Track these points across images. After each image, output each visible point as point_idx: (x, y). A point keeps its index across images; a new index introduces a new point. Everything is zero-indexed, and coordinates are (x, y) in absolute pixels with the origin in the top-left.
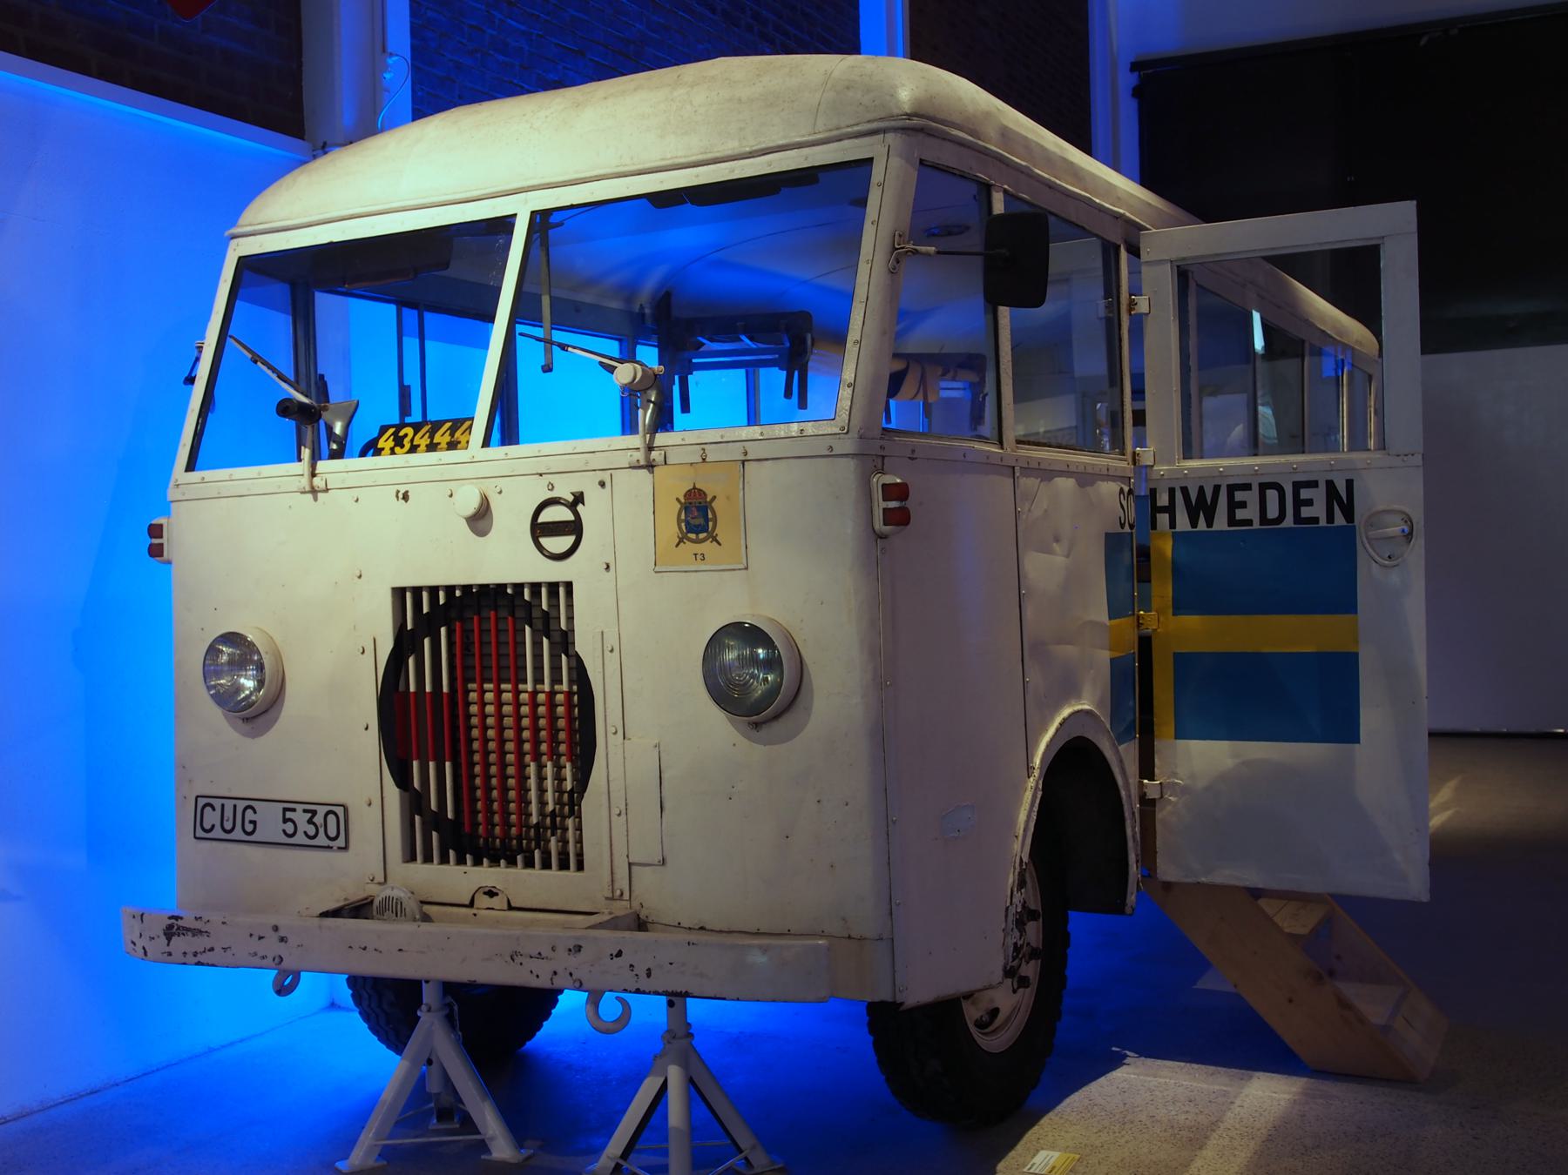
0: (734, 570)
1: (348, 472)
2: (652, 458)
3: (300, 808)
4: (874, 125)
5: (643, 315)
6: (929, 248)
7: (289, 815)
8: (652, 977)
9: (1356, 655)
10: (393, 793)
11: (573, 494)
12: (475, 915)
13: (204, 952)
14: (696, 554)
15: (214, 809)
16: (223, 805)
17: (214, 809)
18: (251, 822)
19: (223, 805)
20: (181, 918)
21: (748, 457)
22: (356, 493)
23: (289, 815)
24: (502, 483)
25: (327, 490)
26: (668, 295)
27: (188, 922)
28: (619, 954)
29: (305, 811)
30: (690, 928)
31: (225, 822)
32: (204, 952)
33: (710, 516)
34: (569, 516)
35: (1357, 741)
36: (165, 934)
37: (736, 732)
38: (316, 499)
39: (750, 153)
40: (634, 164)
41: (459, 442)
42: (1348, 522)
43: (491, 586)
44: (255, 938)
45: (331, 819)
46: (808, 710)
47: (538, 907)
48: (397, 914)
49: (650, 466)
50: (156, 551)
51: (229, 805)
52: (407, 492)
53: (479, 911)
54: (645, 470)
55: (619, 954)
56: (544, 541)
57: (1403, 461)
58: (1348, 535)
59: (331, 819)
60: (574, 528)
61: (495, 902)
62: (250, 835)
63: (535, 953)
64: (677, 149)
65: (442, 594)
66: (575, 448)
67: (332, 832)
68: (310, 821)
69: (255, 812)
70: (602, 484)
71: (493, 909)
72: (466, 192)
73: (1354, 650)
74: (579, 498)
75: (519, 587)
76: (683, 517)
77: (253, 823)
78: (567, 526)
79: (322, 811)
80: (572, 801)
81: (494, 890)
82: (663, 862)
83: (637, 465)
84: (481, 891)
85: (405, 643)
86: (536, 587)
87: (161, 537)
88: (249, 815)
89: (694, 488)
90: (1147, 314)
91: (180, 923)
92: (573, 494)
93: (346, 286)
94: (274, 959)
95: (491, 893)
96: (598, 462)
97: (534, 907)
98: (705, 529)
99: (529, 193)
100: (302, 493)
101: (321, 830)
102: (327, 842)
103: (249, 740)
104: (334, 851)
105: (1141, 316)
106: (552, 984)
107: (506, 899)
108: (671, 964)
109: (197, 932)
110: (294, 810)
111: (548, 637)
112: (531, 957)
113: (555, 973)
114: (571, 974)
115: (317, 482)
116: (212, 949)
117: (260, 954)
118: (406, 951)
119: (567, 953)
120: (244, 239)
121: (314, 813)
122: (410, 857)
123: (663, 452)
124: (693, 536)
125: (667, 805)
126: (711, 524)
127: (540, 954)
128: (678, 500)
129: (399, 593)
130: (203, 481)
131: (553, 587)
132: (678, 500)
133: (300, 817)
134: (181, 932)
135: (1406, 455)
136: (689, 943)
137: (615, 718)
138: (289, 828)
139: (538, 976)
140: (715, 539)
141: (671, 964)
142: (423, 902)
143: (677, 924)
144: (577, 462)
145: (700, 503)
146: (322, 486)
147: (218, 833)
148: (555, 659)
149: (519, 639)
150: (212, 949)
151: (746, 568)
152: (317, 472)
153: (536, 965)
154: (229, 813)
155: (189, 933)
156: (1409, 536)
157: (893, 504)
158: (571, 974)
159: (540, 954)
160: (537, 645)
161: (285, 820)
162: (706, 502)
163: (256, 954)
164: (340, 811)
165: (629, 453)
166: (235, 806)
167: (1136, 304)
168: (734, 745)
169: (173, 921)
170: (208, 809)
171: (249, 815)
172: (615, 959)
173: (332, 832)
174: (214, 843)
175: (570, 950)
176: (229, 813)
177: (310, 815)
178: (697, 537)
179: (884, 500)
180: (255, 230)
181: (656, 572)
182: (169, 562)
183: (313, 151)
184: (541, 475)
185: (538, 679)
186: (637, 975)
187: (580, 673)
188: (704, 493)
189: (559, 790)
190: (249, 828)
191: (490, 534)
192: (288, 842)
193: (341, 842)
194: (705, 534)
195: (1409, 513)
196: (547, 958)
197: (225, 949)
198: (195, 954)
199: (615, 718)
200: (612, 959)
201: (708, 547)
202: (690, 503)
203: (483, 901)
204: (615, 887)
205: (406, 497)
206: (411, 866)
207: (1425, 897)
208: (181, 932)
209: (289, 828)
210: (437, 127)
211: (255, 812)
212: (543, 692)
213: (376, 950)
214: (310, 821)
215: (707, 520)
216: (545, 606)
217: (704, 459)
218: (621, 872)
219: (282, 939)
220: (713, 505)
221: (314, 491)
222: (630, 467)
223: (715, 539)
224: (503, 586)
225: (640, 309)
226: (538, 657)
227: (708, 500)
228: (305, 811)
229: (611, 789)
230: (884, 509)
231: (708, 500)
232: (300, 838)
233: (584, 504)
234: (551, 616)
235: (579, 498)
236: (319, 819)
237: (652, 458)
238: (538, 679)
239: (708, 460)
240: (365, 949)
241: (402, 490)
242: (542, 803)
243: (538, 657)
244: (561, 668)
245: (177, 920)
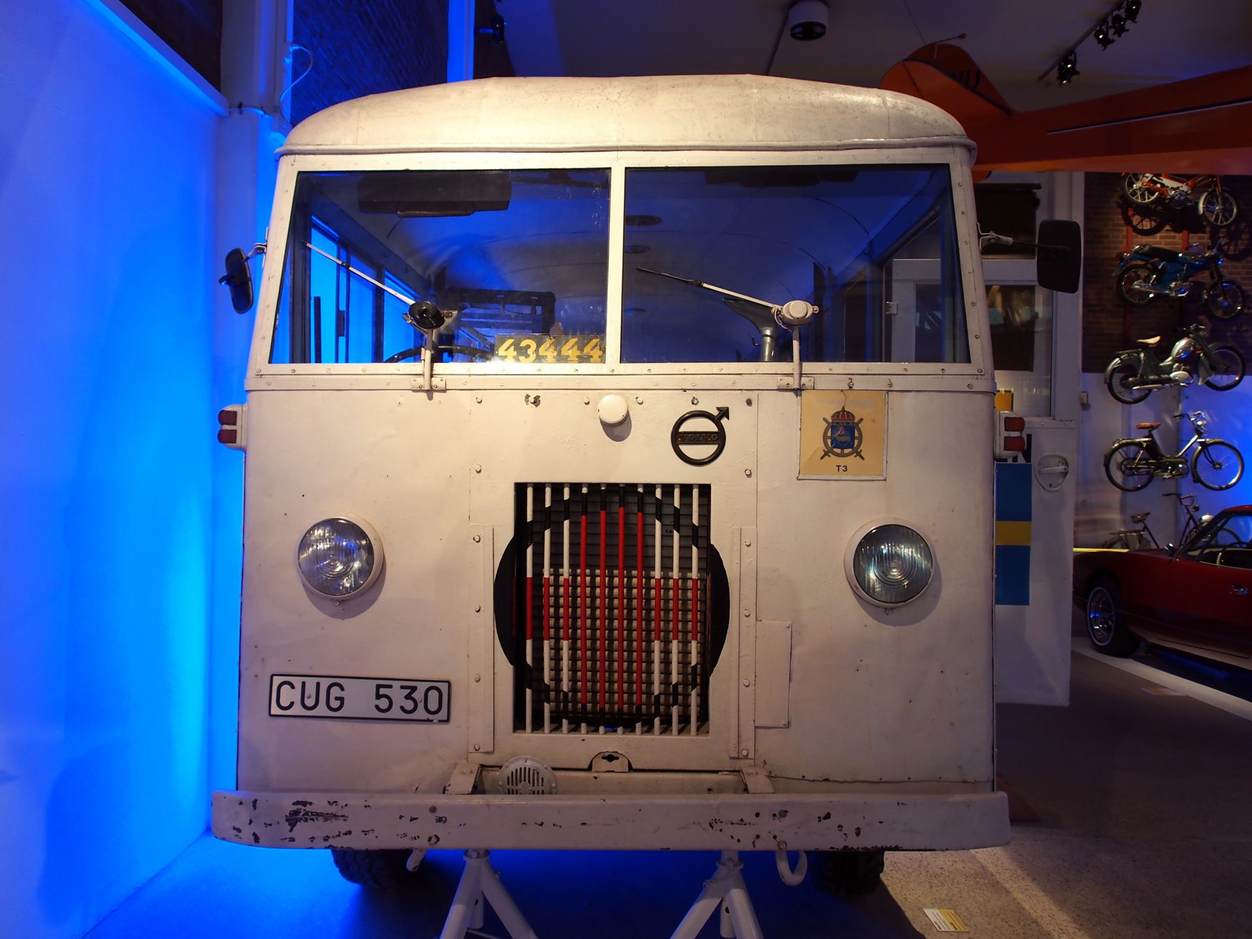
0: (879, 480)
1: (470, 375)
2: (802, 383)
3: (396, 685)
4: (945, 139)
5: (430, 281)
6: (1009, 238)
7: (382, 691)
8: (860, 836)
9: (1029, 547)
10: (506, 670)
11: (718, 409)
12: (596, 778)
13: (339, 836)
14: (839, 466)
15: (293, 687)
16: (304, 684)
17: (293, 687)
18: (337, 698)
19: (304, 684)
20: (311, 804)
21: (892, 389)
22: (480, 394)
23: (382, 691)
24: (642, 396)
25: (444, 391)
26: (445, 268)
27: (319, 803)
28: (828, 816)
29: (402, 687)
30: (814, 780)
31: (306, 699)
32: (339, 836)
33: (856, 435)
34: (712, 427)
35: (1027, 603)
36: (287, 820)
37: (868, 616)
38: (430, 398)
39: (838, 146)
40: (757, 141)
41: (591, 357)
42: (1026, 461)
43: (621, 486)
44: (406, 820)
45: (433, 695)
46: (936, 597)
47: (665, 768)
48: (529, 782)
49: (798, 391)
50: (227, 438)
51: (311, 684)
52: (538, 397)
53: (600, 774)
54: (792, 393)
55: (828, 816)
56: (685, 449)
57: (1065, 424)
58: (1026, 470)
59: (433, 695)
60: (718, 438)
61: (615, 765)
62: (337, 712)
63: (736, 819)
64: (749, 135)
65: (566, 492)
66: (504, 370)
67: (433, 705)
68: (408, 697)
69: (342, 689)
70: (749, 402)
71: (613, 771)
72: (552, 143)
73: (1026, 544)
74: (724, 413)
75: (650, 488)
76: (829, 434)
77: (341, 699)
78: (709, 437)
79: (422, 687)
80: (700, 676)
81: (615, 755)
82: (788, 725)
83: (786, 388)
84: (601, 755)
85: (524, 533)
86: (668, 489)
87: (235, 424)
88: (335, 692)
89: (843, 410)
90: (895, 315)
91: (308, 808)
92: (718, 409)
93: (399, 212)
94: (430, 839)
95: (610, 758)
96: (743, 383)
97: (656, 768)
98: (851, 445)
99: (619, 152)
100: (414, 391)
101: (421, 706)
102: (426, 716)
103: (338, 622)
104: (435, 723)
105: (891, 315)
106: (754, 846)
107: (627, 763)
108: (881, 822)
109: (328, 817)
110: (390, 687)
111: (678, 531)
112: (732, 824)
113: (758, 837)
114: (775, 837)
115: (436, 381)
116: (349, 833)
117: (411, 835)
118: (590, 825)
119: (772, 817)
120: (302, 156)
121: (414, 689)
122: (519, 724)
123: (812, 379)
124: (838, 451)
125: (794, 677)
126: (856, 441)
127: (742, 820)
128: (824, 419)
129: (520, 489)
130: (294, 373)
131: (686, 489)
132: (824, 419)
133: (398, 695)
134: (309, 818)
135: (1067, 421)
136: (898, 803)
137: (748, 601)
138: (384, 703)
139: (739, 841)
140: (859, 454)
141: (881, 822)
142: (554, 769)
143: (801, 778)
144: (726, 382)
145: (848, 423)
146: (441, 385)
147: (297, 709)
148: (685, 549)
149: (648, 531)
150: (349, 833)
151: (885, 480)
152: (434, 373)
153: (738, 831)
154: (311, 690)
155: (319, 818)
156: (1065, 474)
157: (1015, 434)
158: (775, 837)
159: (742, 820)
160: (667, 536)
161: (378, 696)
162: (853, 423)
163: (405, 835)
164: (444, 687)
165: (779, 377)
166: (318, 684)
167: (890, 307)
168: (865, 626)
169: (300, 807)
170: (286, 688)
171: (335, 692)
172: (822, 820)
173: (433, 705)
174: (292, 720)
175: (774, 815)
176: (311, 690)
177: (409, 691)
178: (842, 452)
179: (1006, 430)
180: (317, 150)
181: (798, 480)
182: (243, 450)
183: (230, 108)
184: (685, 390)
185: (667, 567)
186: (845, 834)
187: (712, 561)
188: (853, 415)
189: (684, 662)
190: (335, 704)
191: (626, 440)
192: (383, 715)
193: (442, 715)
194: (850, 450)
195: (1065, 457)
196: (750, 824)
197: (366, 832)
198: (326, 838)
199: (748, 601)
200: (820, 821)
201: (851, 461)
202: (838, 423)
203: (605, 765)
204: (741, 748)
205: (536, 402)
206: (518, 735)
207: (1066, 703)
208: (309, 818)
209: (384, 703)
210: (495, 90)
211: (342, 689)
212: (691, 579)
213: (554, 825)
214: (408, 697)
215: (853, 438)
216: (677, 504)
217: (850, 387)
218: (748, 733)
219: (440, 820)
220: (860, 425)
221: (430, 392)
222: (779, 390)
223: (859, 454)
224: (635, 486)
225: (428, 277)
226: (667, 547)
227: (856, 421)
228: (402, 687)
229: (740, 664)
230: (1005, 437)
231: (856, 421)
232: (395, 712)
233: (728, 418)
234: (681, 513)
235: (724, 413)
236: (420, 695)
237: (802, 383)
238: (667, 567)
239: (854, 388)
240: (542, 824)
241: (533, 394)
242: (666, 672)
243: (667, 547)
244: (691, 558)
245: (305, 806)
